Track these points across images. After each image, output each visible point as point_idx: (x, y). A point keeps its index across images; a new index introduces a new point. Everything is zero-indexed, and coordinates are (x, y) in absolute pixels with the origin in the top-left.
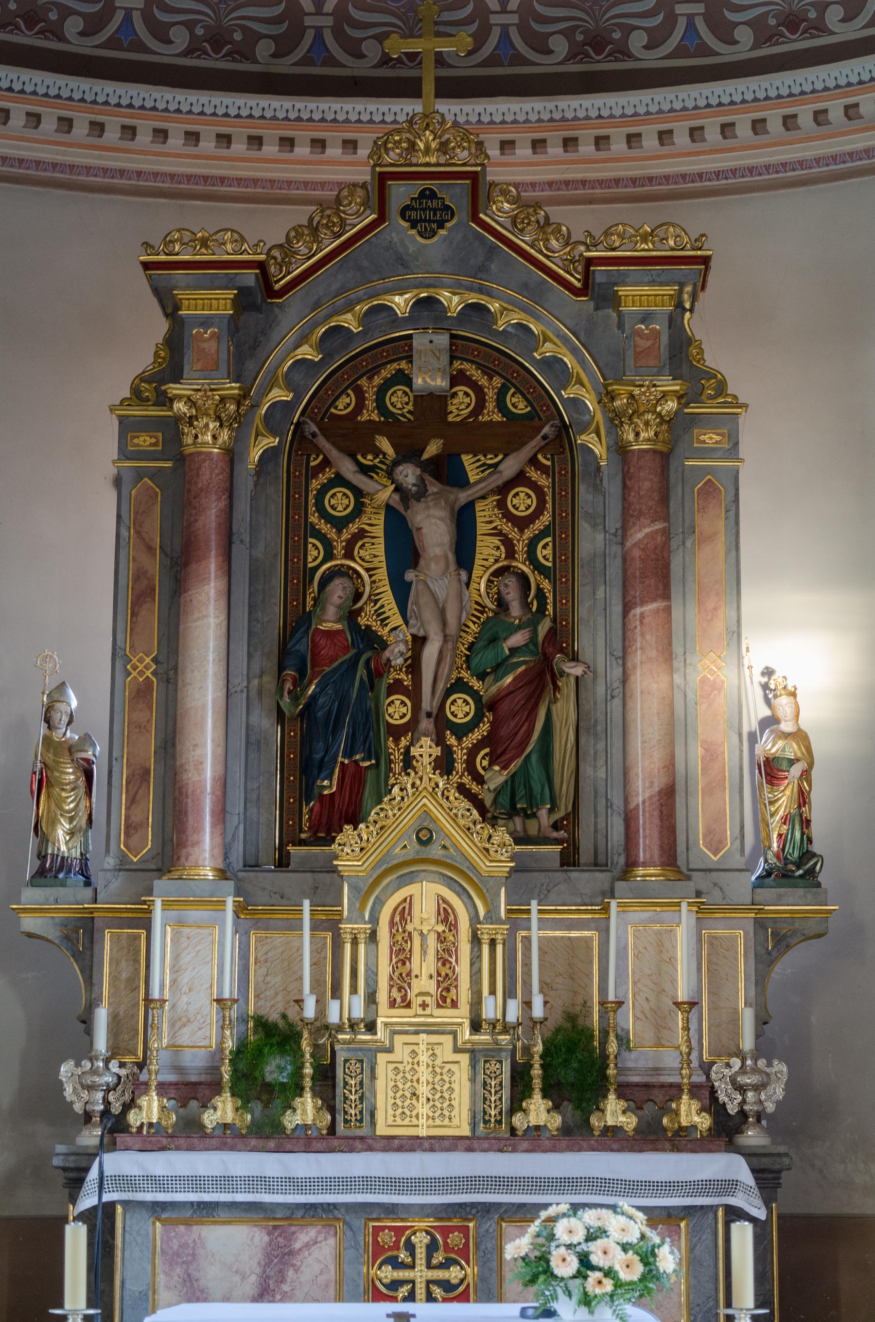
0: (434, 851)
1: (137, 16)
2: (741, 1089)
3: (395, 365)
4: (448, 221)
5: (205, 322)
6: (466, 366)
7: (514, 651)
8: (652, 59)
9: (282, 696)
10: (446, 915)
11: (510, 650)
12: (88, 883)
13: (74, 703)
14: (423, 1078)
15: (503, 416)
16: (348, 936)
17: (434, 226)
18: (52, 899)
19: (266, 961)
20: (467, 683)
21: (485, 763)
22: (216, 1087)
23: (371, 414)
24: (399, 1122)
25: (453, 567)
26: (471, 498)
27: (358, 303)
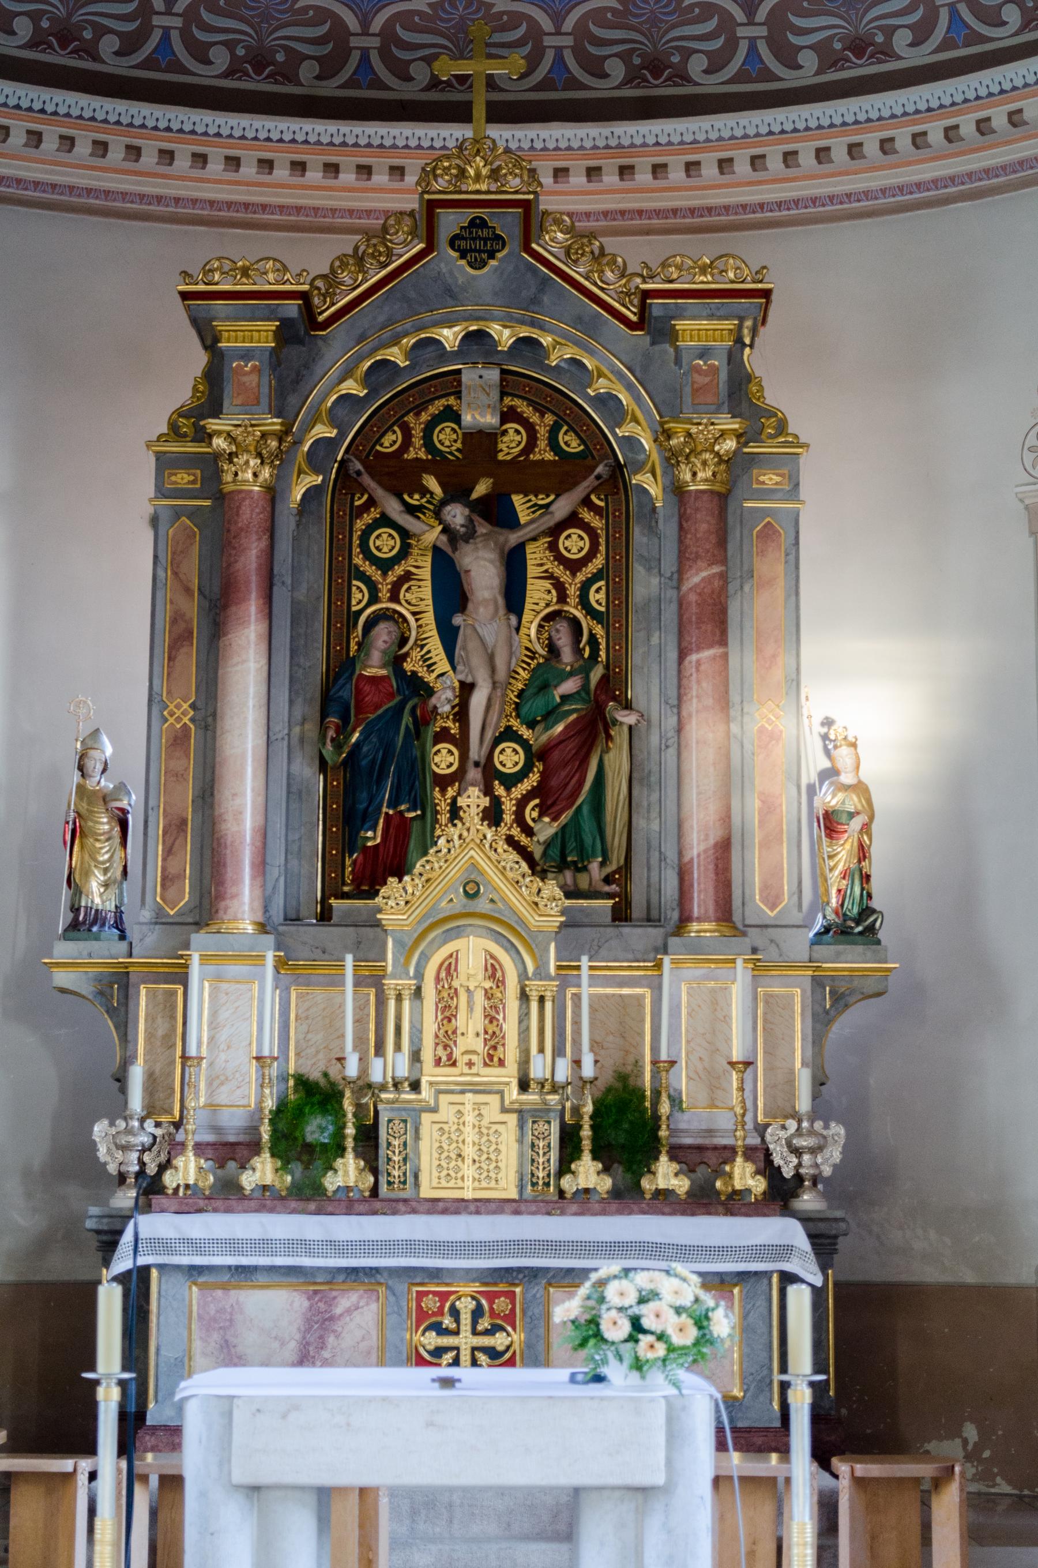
0: (482, 905)
1: (175, 35)
2: (797, 1152)
3: (443, 402)
4: (499, 251)
5: (246, 355)
6: (517, 402)
7: (565, 698)
8: (712, 84)
9: (324, 744)
10: (493, 971)
11: (562, 697)
12: (123, 937)
13: (109, 750)
14: (470, 1140)
15: (556, 454)
16: (392, 992)
17: (485, 256)
18: (85, 953)
19: (307, 1018)
20: (516, 732)
21: (535, 814)
22: (254, 1147)
23: (417, 452)
24: (444, 1184)
25: (502, 611)
26: (521, 540)
27: (404, 336)
